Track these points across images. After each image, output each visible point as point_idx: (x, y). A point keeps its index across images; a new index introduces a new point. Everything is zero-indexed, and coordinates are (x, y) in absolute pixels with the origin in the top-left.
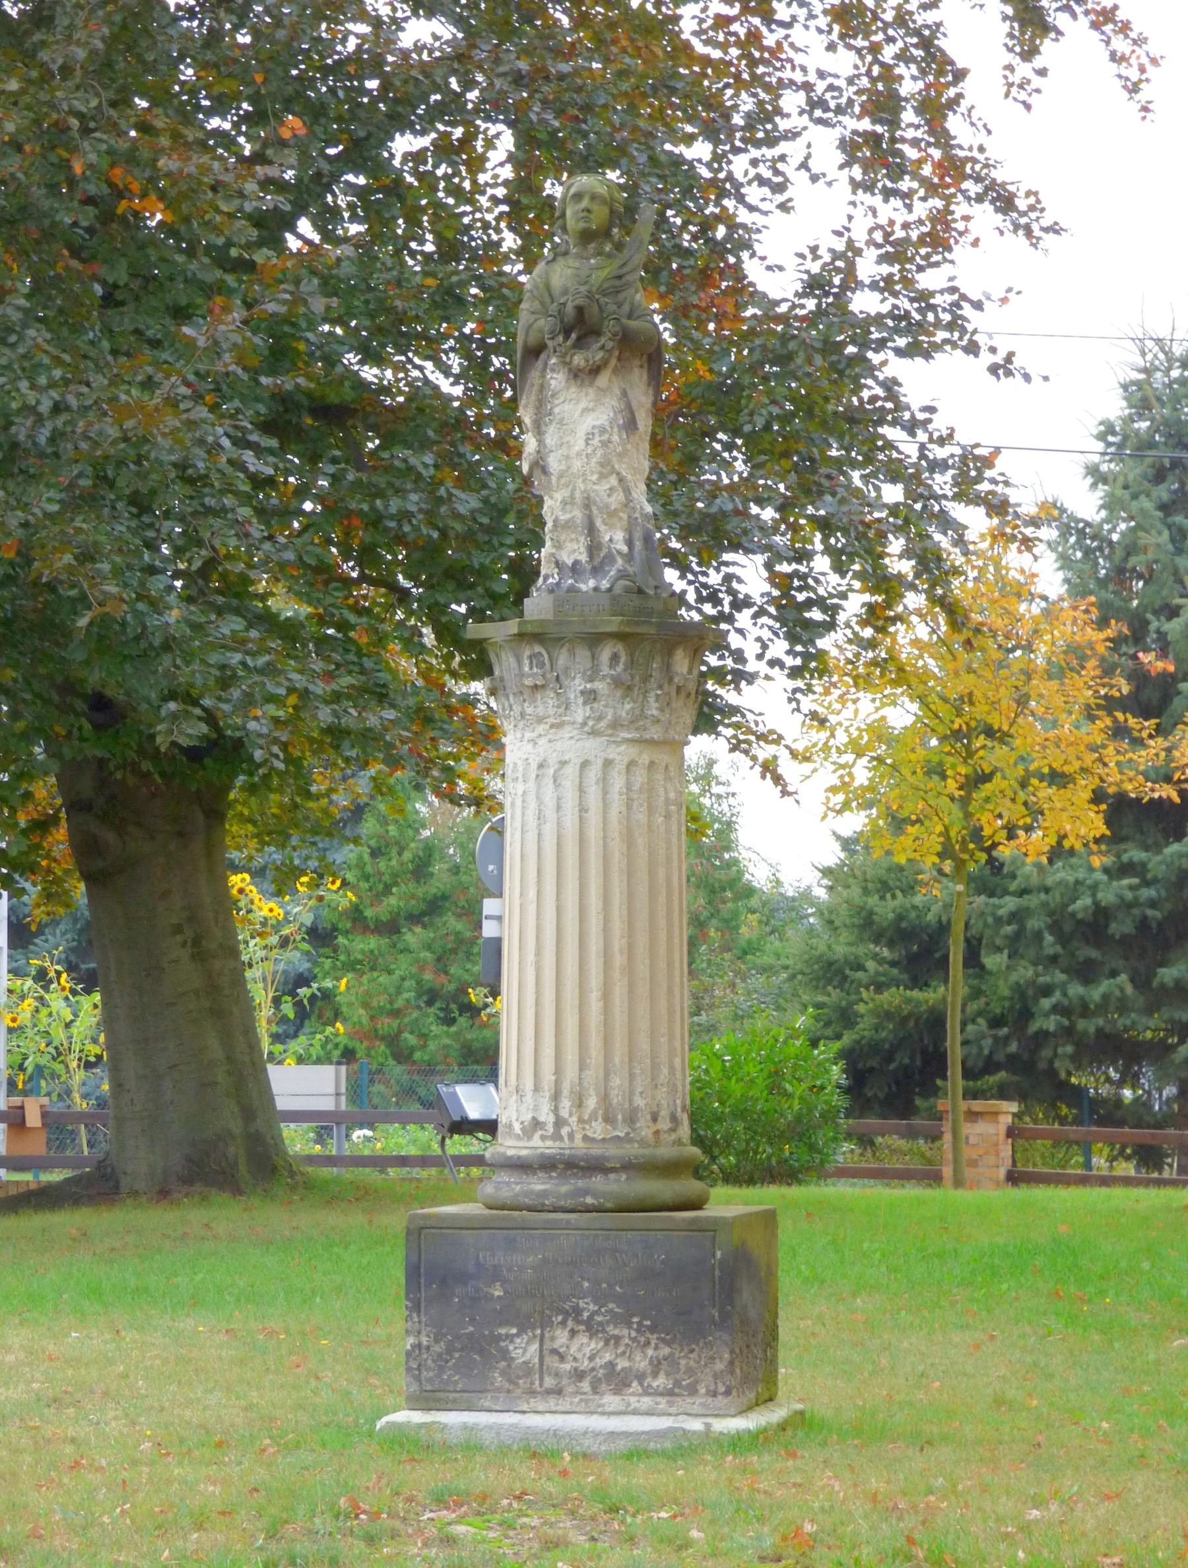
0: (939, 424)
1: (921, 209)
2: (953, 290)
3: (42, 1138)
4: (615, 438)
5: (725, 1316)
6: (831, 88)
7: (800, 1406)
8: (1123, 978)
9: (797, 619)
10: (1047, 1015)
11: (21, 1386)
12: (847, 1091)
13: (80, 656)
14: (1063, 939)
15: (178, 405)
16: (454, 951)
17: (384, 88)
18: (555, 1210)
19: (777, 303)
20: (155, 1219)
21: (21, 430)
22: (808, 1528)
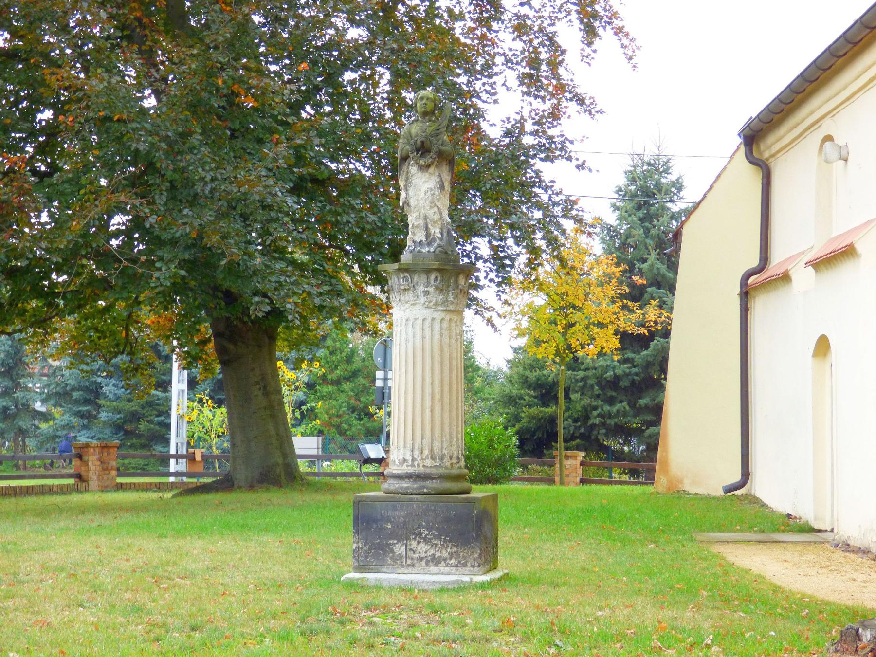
0: (556, 188)
1: (548, 105)
2: (562, 136)
3: (202, 465)
4: (436, 193)
5: (478, 536)
6: (514, 55)
7: (506, 571)
8: (625, 403)
9: (501, 261)
10: (595, 418)
11: (201, 563)
12: (519, 447)
13: (221, 276)
14: (602, 388)
15: (261, 179)
16: (362, 391)
17: (340, 54)
18: (412, 494)
19: (494, 140)
20: (248, 497)
21: (198, 188)
22: (512, 619)
